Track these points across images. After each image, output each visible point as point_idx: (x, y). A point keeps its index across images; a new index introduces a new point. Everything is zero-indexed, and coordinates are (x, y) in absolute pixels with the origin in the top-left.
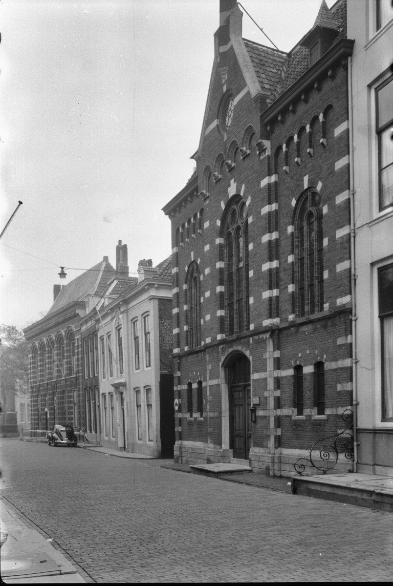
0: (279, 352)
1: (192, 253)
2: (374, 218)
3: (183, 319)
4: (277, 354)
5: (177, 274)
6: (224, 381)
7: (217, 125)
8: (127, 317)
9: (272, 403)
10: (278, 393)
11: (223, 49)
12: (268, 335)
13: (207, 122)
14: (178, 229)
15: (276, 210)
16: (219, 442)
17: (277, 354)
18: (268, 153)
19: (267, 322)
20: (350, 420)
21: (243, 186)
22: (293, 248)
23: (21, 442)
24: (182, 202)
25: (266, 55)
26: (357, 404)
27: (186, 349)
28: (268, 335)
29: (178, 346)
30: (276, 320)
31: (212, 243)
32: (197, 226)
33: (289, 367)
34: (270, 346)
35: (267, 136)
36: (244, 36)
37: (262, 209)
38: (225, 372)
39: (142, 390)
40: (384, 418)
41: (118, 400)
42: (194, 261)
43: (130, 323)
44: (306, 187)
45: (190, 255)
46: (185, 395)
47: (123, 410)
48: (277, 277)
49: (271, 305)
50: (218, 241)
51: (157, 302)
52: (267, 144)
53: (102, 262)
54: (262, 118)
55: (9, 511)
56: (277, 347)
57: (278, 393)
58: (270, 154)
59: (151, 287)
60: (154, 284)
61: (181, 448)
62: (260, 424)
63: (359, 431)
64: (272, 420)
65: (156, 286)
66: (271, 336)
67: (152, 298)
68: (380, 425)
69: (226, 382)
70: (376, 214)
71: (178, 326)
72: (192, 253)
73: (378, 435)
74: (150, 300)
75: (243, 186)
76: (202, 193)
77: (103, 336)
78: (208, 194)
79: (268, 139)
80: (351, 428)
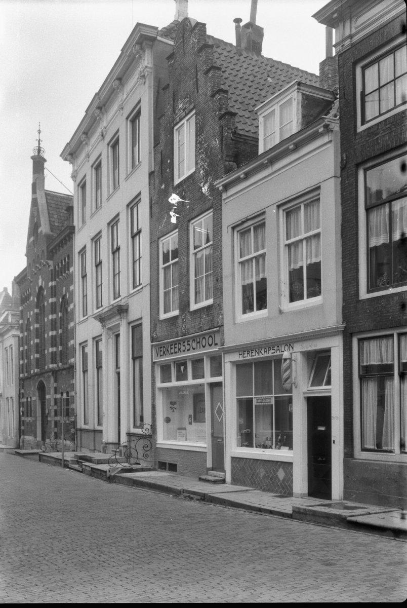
0: (56, 384)
1: (64, 288)
2: (95, 313)
4: (55, 385)
5: (22, 324)
6: (38, 399)
7: (33, 240)
8: (3, 345)
9: (53, 414)
10: (55, 407)
12: (50, 374)
16: (35, 437)
17: (55, 385)
18: (52, 268)
19: (51, 366)
20: (74, 423)
22: (61, 326)
23: (399, 307)
25: (62, 200)
26: (76, 416)
27: (26, 375)
28: (50, 374)
29: (23, 373)
30: (55, 365)
34: (52, 380)
35: (51, 258)
36: (46, 188)
38: (39, 392)
39: (10, 399)
40: (85, 423)
43: (4, 350)
46: (25, 404)
47: (119, 374)
50: (36, 311)
51: (17, 338)
52: (51, 262)
53: (3, 292)
54: (47, 248)
55: (347, 594)
56: (56, 381)
57: (55, 407)
58: (53, 268)
59: (13, 328)
61: (23, 440)
62: (49, 423)
63: (77, 430)
64: (53, 423)
65: (16, 327)
66: (53, 374)
67: (14, 336)
68: (84, 427)
69: (39, 399)
70: (132, 291)
71: (23, 360)
72: (64, 288)
73: (83, 432)
74: (13, 336)
77: (12, 345)
78: (31, 280)
79: (52, 260)
80: (74, 428)
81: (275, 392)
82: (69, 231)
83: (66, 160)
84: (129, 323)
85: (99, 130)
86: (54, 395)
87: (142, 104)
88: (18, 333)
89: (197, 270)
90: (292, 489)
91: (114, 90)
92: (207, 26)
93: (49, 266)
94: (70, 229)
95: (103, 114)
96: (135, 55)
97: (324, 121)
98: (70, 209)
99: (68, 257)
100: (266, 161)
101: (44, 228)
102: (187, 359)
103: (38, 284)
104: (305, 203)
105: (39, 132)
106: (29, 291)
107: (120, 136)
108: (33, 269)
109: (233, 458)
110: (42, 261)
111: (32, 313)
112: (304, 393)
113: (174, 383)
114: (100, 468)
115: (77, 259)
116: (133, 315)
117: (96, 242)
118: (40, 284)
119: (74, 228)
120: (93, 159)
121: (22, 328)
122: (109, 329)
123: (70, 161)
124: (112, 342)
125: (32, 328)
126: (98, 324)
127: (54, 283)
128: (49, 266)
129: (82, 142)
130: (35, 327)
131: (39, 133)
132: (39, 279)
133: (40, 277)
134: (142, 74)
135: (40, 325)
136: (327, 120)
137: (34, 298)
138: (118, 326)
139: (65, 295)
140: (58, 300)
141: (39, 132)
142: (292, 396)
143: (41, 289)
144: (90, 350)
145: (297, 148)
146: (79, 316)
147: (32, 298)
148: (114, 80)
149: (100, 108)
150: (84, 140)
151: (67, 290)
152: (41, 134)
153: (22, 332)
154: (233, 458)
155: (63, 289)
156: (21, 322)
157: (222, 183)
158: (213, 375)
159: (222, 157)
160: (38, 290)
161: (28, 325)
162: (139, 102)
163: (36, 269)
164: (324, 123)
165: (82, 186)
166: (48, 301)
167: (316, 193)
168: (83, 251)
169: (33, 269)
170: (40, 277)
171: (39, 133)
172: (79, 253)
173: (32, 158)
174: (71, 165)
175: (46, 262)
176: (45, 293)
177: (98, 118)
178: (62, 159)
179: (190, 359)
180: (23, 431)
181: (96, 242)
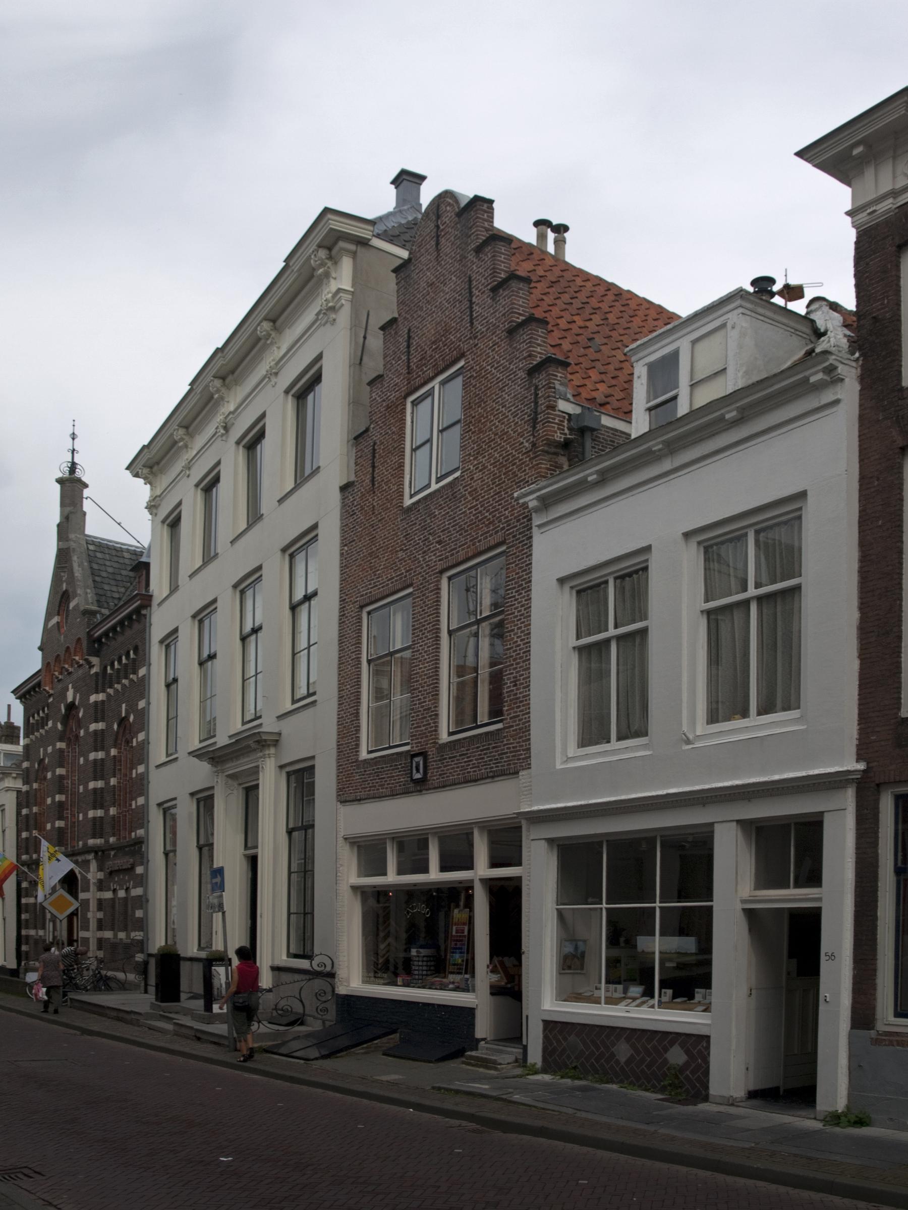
1: (124, 706)
3: (32, 822)
7: (58, 622)
11: (64, 545)
13: (48, 616)
14: (105, 668)
15: (102, 730)
19: (91, 842)
21: (78, 695)
24: (102, 638)
28: (91, 857)
29: (27, 853)
31: (54, 746)
32: (122, 674)
33: (109, 890)
34: (93, 866)
35: (97, 653)
37: (91, 726)
41: (753, 996)
42: (125, 717)
44: (123, 715)
45: (40, 752)
48: (102, 797)
49: (94, 824)
51: (14, 794)
52: (95, 660)
57: (100, 915)
58: (98, 671)
60: (11, 773)
67: (8, 789)
72: (124, 706)
75: (78, 695)
76: (45, 690)
79: (98, 656)
81: (661, 897)
82: (139, 602)
83: (136, 475)
84: (281, 767)
85: (219, 418)
86: (99, 893)
87: (222, 467)
88: (19, 784)
89: (709, 593)
90: (707, 1088)
91: (175, 443)
92: (495, 205)
93: (91, 666)
94: (141, 599)
95: (229, 388)
96: (314, 269)
97: (827, 359)
98: (145, 567)
99: (136, 650)
100: (660, 446)
101: (83, 599)
102: (428, 834)
103: (65, 697)
104: (706, 544)
105: (74, 437)
106: (43, 711)
107: (221, 471)
108: (56, 673)
109: (546, 1023)
110: (77, 658)
111: (50, 749)
112: (744, 901)
113: (392, 877)
114: (216, 1032)
115: (156, 653)
116: (292, 752)
117: (168, 647)
118: (70, 699)
119: (150, 597)
120: (199, 471)
121: (28, 777)
122: (232, 777)
123: (145, 479)
124: (237, 799)
125: (49, 775)
126: (204, 767)
127: (101, 697)
128: (91, 666)
129: (175, 443)
130: (57, 773)
131: (73, 439)
132: (68, 690)
133: (70, 686)
134: (330, 304)
135: (67, 771)
136: (834, 357)
137: (55, 724)
138: (255, 771)
139: (126, 718)
140: (110, 726)
141: (74, 437)
142: (711, 907)
143: (71, 707)
144: (186, 811)
145: (603, 480)
146: (158, 753)
147: (50, 723)
148: (261, 322)
149: (273, 320)
150: (323, 264)
151: (132, 708)
152: (76, 440)
153: (26, 782)
154: (546, 1023)
155: (121, 707)
156: (25, 765)
157: (538, 494)
158: (495, 863)
159: (534, 445)
160: (66, 710)
161: (43, 768)
162: (218, 463)
163: (61, 673)
164: (827, 364)
165: (174, 523)
166: (87, 729)
167: (642, 558)
168: (170, 640)
169: (56, 673)
170: (70, 686)
171: (73, 439)
172: (161, 642)
173: (60, 481)
174: (148, 486)
175: (86, 660)
176: (81, 715)
177: (216, 396)
178: (130, 474)
179: (436, 833)
180: (27, 953)
181: (168, 647)
